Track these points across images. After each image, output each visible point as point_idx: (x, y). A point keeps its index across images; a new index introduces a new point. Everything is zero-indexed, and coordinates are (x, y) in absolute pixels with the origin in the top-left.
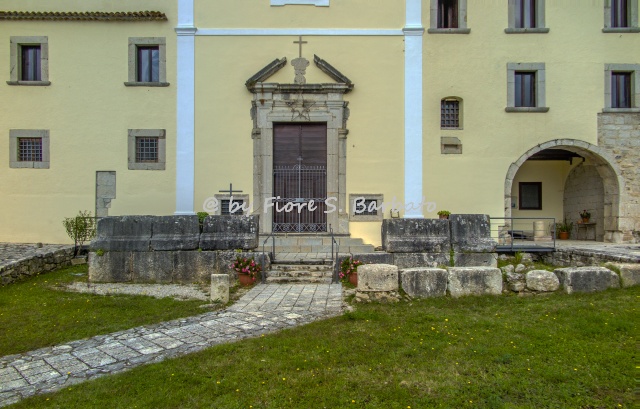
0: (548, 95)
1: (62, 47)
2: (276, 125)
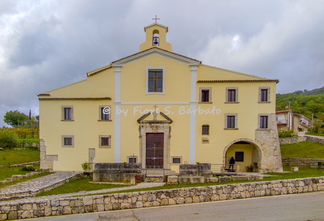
0: (238, 124)
1: (78, 109)
2: (147, 134)
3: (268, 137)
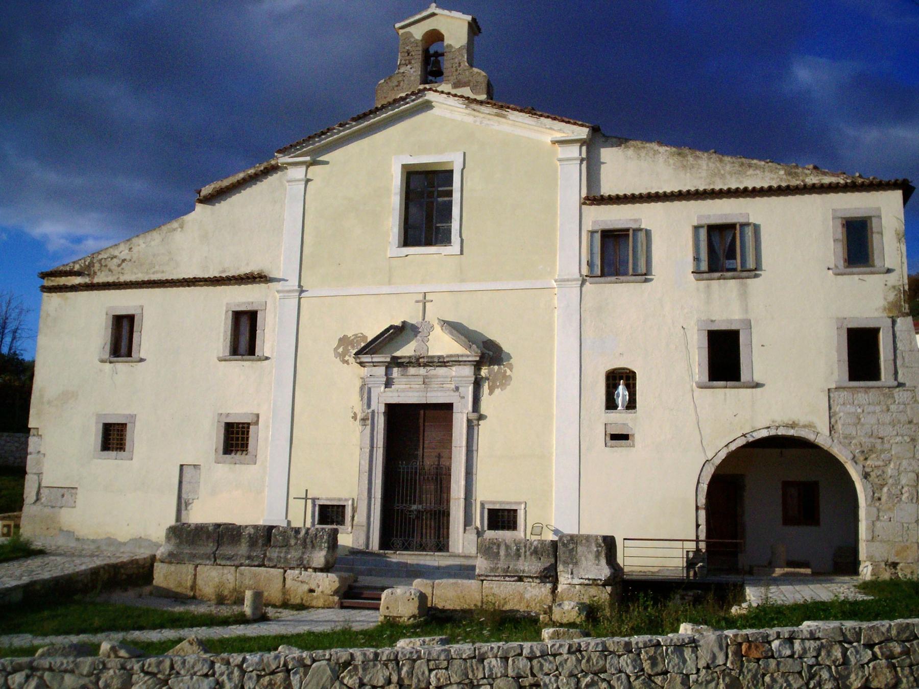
0: (755, 359)
3: (887, 418)
